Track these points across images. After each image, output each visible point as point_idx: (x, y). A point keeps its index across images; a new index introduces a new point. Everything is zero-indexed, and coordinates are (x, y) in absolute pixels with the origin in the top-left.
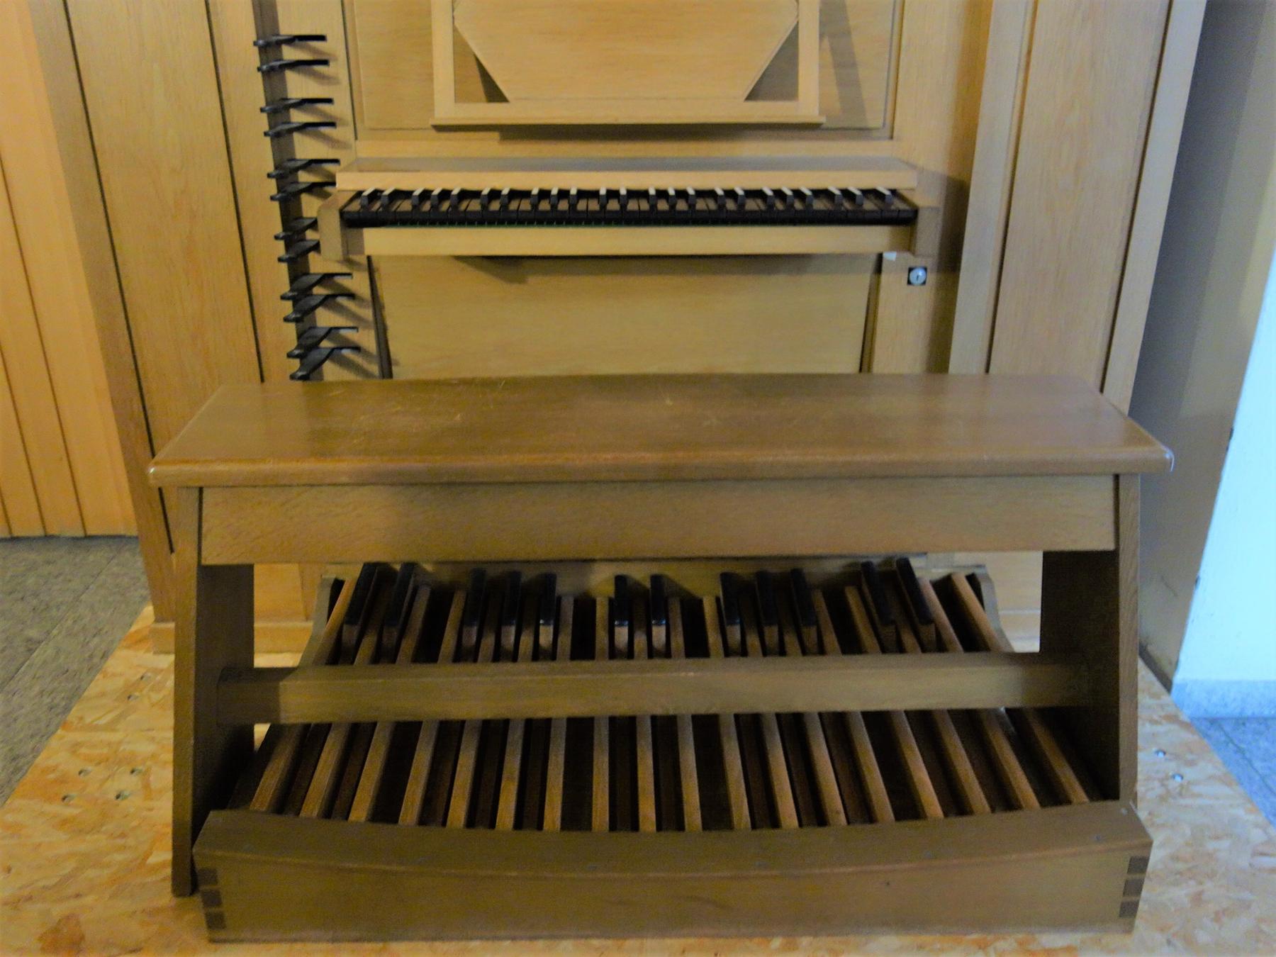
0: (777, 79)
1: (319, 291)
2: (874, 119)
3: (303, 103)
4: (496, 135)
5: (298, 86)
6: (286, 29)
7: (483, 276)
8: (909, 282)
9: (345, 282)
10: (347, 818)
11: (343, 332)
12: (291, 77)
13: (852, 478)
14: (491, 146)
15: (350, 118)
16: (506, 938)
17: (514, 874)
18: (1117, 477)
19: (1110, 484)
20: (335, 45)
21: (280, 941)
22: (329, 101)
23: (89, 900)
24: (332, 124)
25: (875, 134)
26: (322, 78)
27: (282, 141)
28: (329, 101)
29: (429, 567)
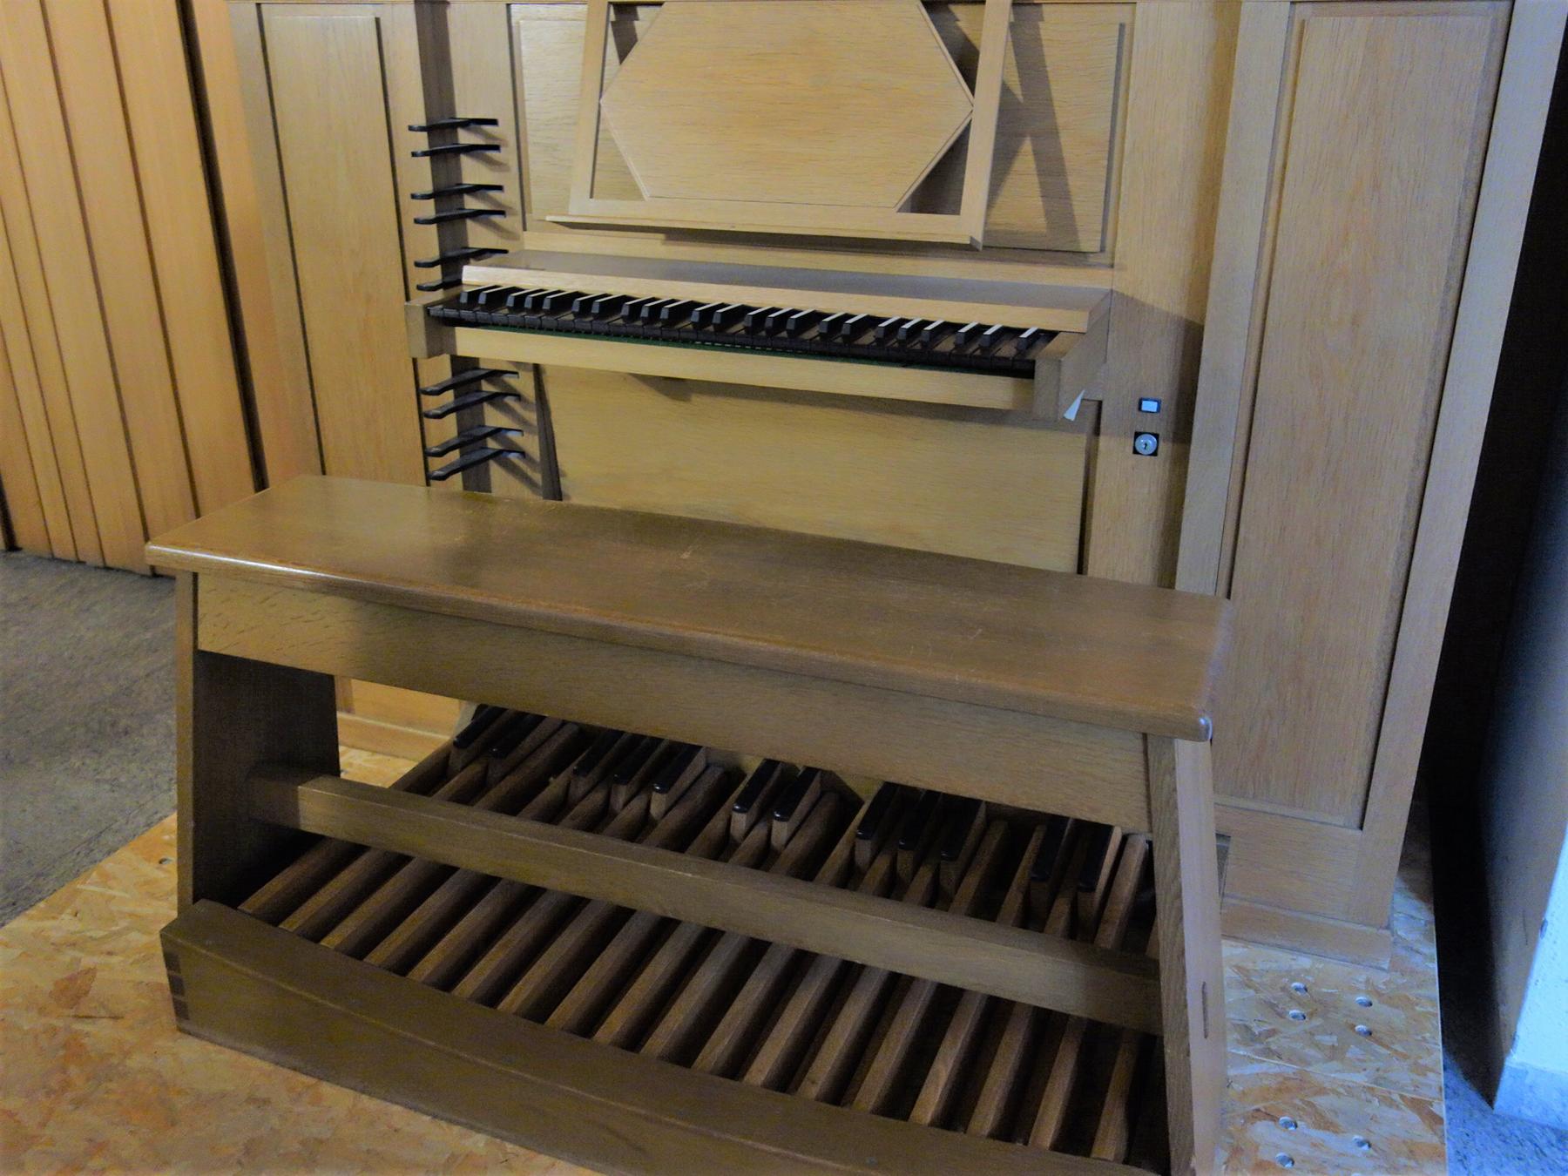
0: (936, 191)
1: (487, 387)
2: (1088, 241)
3: (475, 190)
4: (661, 236)
5: (472, 171)
6: (462, 113)
7: (644, 387)
8: (1135, 452)
9: (511, 380)
11: (510, 435)
12: (466, 161)
13: (816, 678)
14: (655, 248)
15: (518, 208)
16: (427, 1114)
17: (432, 1043)
18: (1145, 736)
19: (1138, 744)
20: (504, 131)
21: (231, 1048)
22: (499, 188)
23: (115, 960)
24: (502, 213)
25: (1092, 260)
28: (499, 188)
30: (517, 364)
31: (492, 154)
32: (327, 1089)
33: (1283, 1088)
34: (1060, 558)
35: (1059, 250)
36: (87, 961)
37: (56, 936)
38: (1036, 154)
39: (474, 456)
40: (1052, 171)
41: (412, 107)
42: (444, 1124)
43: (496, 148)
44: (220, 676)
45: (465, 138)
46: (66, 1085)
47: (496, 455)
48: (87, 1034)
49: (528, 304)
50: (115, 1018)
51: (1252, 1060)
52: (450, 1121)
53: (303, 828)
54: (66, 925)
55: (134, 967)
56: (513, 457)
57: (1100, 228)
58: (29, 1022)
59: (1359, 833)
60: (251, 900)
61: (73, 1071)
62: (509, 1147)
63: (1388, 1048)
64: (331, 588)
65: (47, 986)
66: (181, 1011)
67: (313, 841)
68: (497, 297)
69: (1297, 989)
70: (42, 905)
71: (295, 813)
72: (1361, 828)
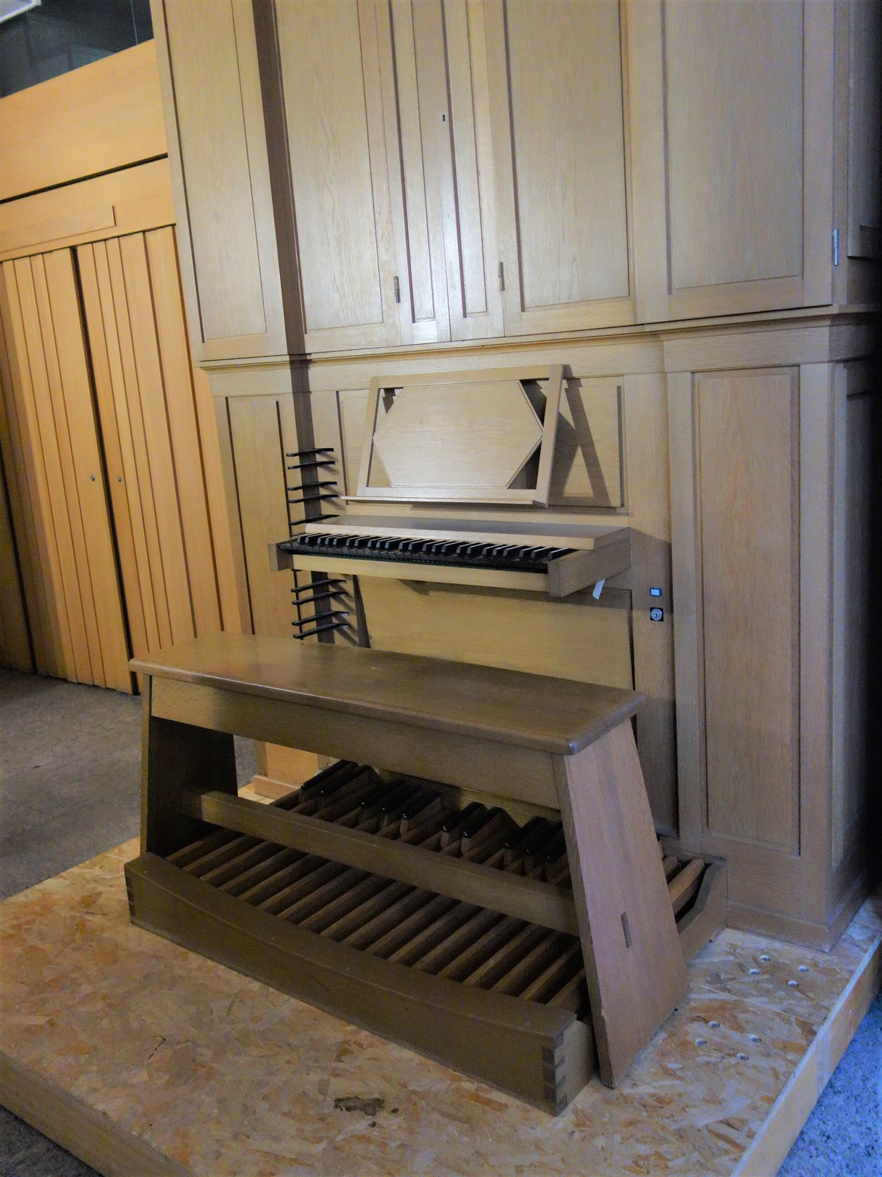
1: (332, 589)
2: (615, 502)
3: (325, 484)
5: (323, 475)
6: (318, 445)
8: (652, 619)
10: (199, 877)
12: (320, 470)
14: (408, 512)
16: (236, 971)
20: (336, 454)
22: (335, 483)
23: (112, 889)
26: (332, 471)
27: (673, 861)
29: (377, 771)
30: (345, 575)
31: (331, 466)
32: (192, 955)
33: (722, 1007)
34: (626, 684)
35: (598, 505)
36: (100, 889)
37: (89, 877)
38: (584, 455)
39: (326, 626)
40: (592, 463)
41: (292, 446)
42: (243, 976)
43: (333, 463)
44: (165, 734)
45: (319, 458)
46: (72, 941)
47: (337, 626)
48: (89, 921)
49: (327, 542)
50: (104, 915)
51: (710, 992)
52: (246, 975)
53: (205, 820)
54: (97, 871)
55: (116, 892)
56: (345, 628)
57: (619, 494)
58: (64, 913)
59: (798, 858)
60: (172, 856)
61: (78, 936)
62: (271, 989)
63: (803, 993)
64: (203, 682)
65: (77, 897)
66: (132, 910)
67: (212, 828)
68: (313, 539)
69: (764, 959)
70: (87, 862)
71: (200, 811)
72: (800, 854)
